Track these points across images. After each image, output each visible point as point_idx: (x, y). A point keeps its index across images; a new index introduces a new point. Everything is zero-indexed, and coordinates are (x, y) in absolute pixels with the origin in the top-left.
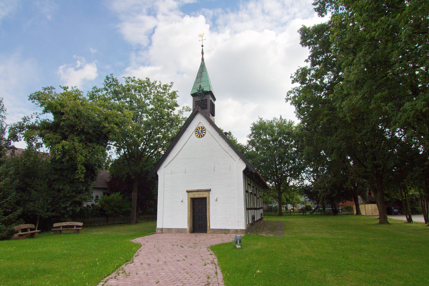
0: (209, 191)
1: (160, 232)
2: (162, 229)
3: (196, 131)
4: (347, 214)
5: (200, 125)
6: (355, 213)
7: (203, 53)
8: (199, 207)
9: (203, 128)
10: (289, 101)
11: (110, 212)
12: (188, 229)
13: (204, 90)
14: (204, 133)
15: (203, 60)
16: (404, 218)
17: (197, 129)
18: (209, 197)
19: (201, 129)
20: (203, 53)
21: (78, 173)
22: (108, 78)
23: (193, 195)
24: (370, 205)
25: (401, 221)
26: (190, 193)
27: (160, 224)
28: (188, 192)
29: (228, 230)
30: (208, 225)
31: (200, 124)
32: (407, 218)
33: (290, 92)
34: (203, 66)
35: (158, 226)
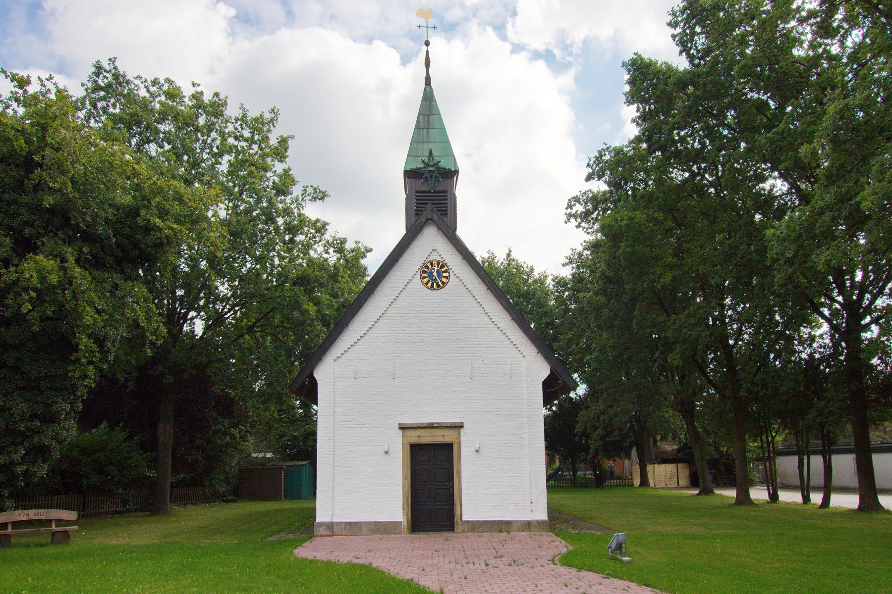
0: (459, 427)
1: (328, 533)
2: (330, 526)
3: (424, 272)
4: (618, 486)
5: (435, 257)
6: (637, 481)
7: (427, 63)
8: (432, 471)
9: (442, 267)
10: (572, 220)
11: (95, 479)
12: (405, 523)
13: (441, 165)
14: (444, 280)
16: (732, 493)
17: (427, 267)
18: (459, 444)
20: (427, 63)
21: (78, 360)
22: (99, 70)
23: (415, 437)
24: (663, 466)
25: (727, 497)
27: (326, 509)
28: (403, 428)
29: (509, 523)
30: (457, 512)
31: (435, 253)
32: (769, 492)
33: (576, 199)
34: (428, 98)
35: (322, 516)
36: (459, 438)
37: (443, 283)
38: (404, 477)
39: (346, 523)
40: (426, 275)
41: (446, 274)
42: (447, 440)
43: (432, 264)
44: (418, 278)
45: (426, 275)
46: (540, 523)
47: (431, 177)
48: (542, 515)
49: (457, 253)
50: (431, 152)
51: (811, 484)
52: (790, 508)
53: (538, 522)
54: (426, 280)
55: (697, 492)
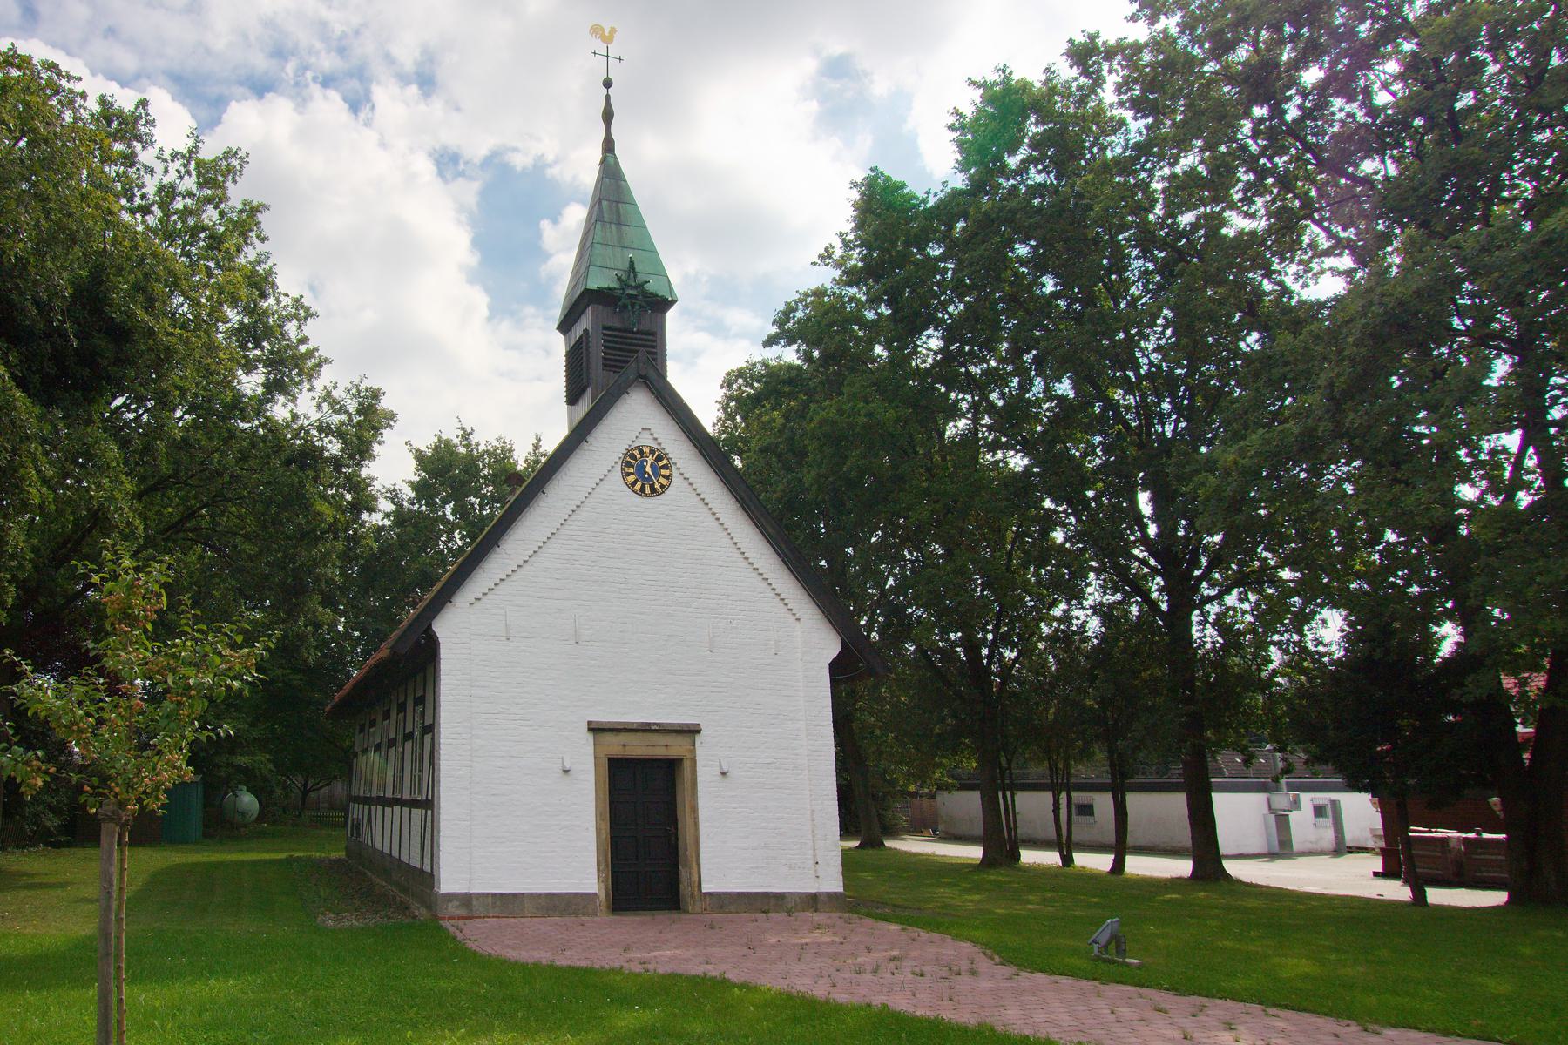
0: (692, 731)
1: (463, 912)
3: (629, 464)
5: (645, 440)
7: (608, 116)
8: (645, 797)
9: (659, 459)
12: (602, 896)
13: (649, 288)
15: (608, 145)
17: (633, 457)
18: (694, 761)
19: (650, 460)
23: (615, 746)
26: (609, 738)
28: (596, 729)
29: (779, 898)
36: (693, 751)
37: (662, 486)
38: (599, 815)
39: (494, 895)
40: (631, 470)
41: (666, 472)
42: (673, 753)
43: (641, 452)
44: (617, 473)
45: (631, 470)
46: (832, 896)
47: (633, 305)
48: (832, 881)
49: (684, 437)
50: (632, 263)
51: (1075, 838)
52: (1092, 877)
53: (829, 895)
54: (631, 479)
55: (856, 843)
